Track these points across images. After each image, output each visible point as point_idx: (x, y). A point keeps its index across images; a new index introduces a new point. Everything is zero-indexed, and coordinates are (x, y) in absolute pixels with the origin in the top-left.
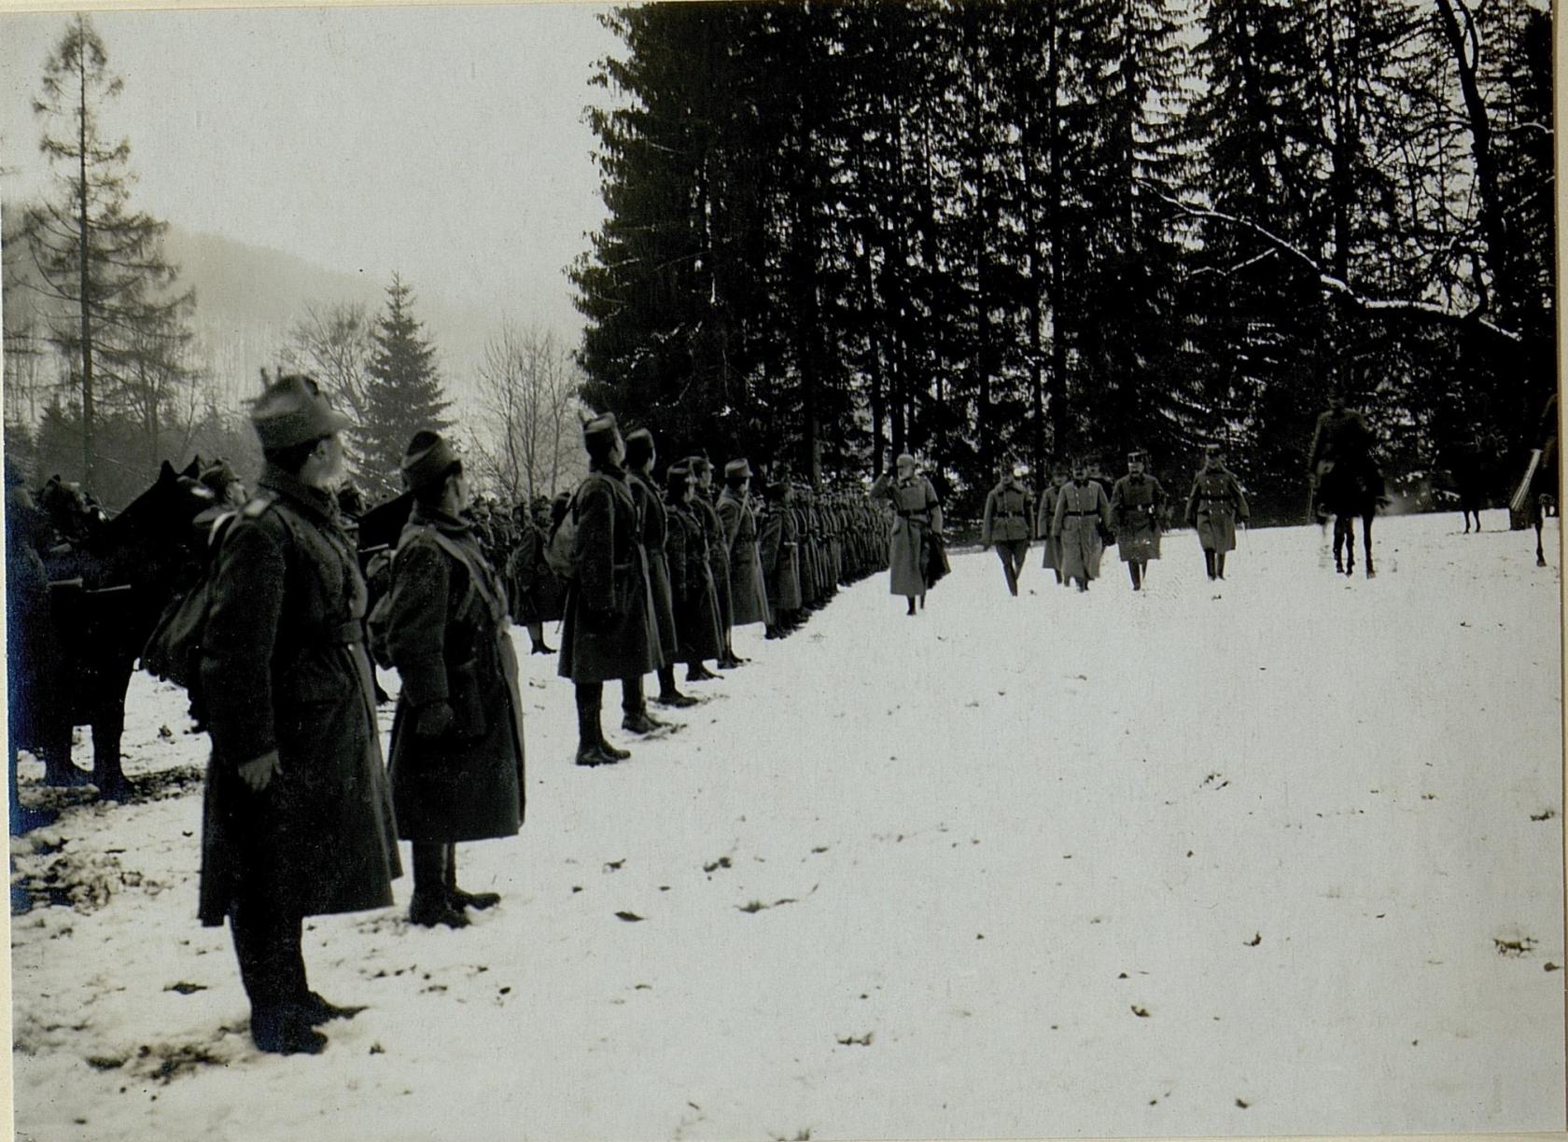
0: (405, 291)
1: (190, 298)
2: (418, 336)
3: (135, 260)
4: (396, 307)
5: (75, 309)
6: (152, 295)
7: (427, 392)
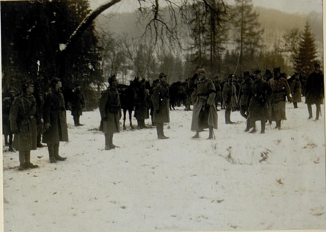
0: (309, 27)
1: (263, 31)
2: (311, 37)
3: (252, 23)
4: (306, 30)
5: (239, 34)
6: (255, 30)
7: (312, 49)
